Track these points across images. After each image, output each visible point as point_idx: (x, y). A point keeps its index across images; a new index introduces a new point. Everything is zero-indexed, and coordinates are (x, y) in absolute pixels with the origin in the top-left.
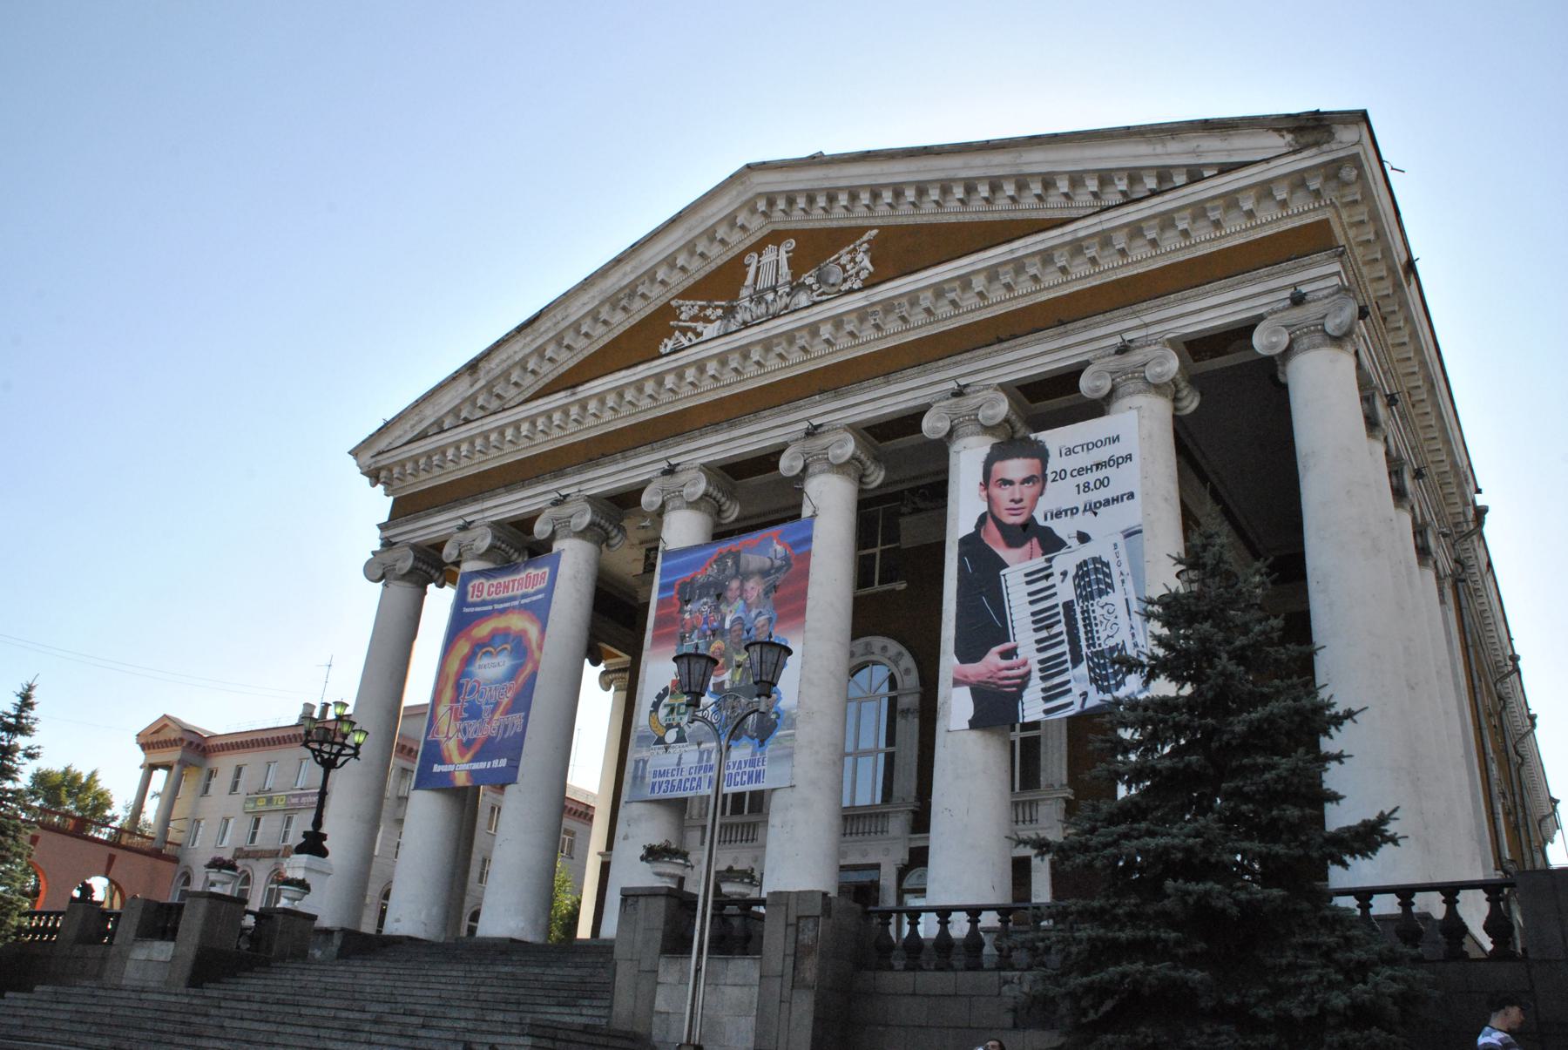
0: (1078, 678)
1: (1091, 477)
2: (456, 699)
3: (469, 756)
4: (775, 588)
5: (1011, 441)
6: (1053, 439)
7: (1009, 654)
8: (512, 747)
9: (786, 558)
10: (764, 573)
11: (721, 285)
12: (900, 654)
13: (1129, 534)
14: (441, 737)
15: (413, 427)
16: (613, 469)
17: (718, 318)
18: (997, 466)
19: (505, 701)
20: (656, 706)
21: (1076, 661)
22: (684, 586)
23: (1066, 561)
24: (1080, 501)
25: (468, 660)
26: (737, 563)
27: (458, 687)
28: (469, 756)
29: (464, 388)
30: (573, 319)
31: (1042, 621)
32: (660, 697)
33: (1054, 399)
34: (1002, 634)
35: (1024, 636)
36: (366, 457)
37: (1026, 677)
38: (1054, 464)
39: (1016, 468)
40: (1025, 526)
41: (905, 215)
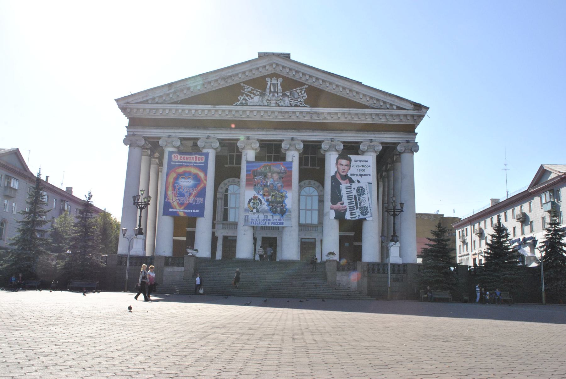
1: (361, 168)
3: (183, 207)
4: (283, 178)
6: (353, 157)
7: (342, 204)
8: (201, 207)
9: (285, 170)
10: (279, 173)
11: (259, 84)
13: (369, 183)
14: (171, 201)
16: (227, 132)
17: (258, 95)
18: (340, 160)
19: (194, 193)
20: (249, 202)
21: (357, 208)
24: (358, 173)
25: (176, 179)
26: (270, 168)
27: (174, 188)
28: (183, 207)
29: (165, 90)
30: (209, 80)
31: (349, 198)
33: (351, 149)
34: (340, 199)
35: (345, 201)
37: (346, 210)
38: (353, 163)
39: (344, 162)
40: (345, 176)
41: (316, 85)
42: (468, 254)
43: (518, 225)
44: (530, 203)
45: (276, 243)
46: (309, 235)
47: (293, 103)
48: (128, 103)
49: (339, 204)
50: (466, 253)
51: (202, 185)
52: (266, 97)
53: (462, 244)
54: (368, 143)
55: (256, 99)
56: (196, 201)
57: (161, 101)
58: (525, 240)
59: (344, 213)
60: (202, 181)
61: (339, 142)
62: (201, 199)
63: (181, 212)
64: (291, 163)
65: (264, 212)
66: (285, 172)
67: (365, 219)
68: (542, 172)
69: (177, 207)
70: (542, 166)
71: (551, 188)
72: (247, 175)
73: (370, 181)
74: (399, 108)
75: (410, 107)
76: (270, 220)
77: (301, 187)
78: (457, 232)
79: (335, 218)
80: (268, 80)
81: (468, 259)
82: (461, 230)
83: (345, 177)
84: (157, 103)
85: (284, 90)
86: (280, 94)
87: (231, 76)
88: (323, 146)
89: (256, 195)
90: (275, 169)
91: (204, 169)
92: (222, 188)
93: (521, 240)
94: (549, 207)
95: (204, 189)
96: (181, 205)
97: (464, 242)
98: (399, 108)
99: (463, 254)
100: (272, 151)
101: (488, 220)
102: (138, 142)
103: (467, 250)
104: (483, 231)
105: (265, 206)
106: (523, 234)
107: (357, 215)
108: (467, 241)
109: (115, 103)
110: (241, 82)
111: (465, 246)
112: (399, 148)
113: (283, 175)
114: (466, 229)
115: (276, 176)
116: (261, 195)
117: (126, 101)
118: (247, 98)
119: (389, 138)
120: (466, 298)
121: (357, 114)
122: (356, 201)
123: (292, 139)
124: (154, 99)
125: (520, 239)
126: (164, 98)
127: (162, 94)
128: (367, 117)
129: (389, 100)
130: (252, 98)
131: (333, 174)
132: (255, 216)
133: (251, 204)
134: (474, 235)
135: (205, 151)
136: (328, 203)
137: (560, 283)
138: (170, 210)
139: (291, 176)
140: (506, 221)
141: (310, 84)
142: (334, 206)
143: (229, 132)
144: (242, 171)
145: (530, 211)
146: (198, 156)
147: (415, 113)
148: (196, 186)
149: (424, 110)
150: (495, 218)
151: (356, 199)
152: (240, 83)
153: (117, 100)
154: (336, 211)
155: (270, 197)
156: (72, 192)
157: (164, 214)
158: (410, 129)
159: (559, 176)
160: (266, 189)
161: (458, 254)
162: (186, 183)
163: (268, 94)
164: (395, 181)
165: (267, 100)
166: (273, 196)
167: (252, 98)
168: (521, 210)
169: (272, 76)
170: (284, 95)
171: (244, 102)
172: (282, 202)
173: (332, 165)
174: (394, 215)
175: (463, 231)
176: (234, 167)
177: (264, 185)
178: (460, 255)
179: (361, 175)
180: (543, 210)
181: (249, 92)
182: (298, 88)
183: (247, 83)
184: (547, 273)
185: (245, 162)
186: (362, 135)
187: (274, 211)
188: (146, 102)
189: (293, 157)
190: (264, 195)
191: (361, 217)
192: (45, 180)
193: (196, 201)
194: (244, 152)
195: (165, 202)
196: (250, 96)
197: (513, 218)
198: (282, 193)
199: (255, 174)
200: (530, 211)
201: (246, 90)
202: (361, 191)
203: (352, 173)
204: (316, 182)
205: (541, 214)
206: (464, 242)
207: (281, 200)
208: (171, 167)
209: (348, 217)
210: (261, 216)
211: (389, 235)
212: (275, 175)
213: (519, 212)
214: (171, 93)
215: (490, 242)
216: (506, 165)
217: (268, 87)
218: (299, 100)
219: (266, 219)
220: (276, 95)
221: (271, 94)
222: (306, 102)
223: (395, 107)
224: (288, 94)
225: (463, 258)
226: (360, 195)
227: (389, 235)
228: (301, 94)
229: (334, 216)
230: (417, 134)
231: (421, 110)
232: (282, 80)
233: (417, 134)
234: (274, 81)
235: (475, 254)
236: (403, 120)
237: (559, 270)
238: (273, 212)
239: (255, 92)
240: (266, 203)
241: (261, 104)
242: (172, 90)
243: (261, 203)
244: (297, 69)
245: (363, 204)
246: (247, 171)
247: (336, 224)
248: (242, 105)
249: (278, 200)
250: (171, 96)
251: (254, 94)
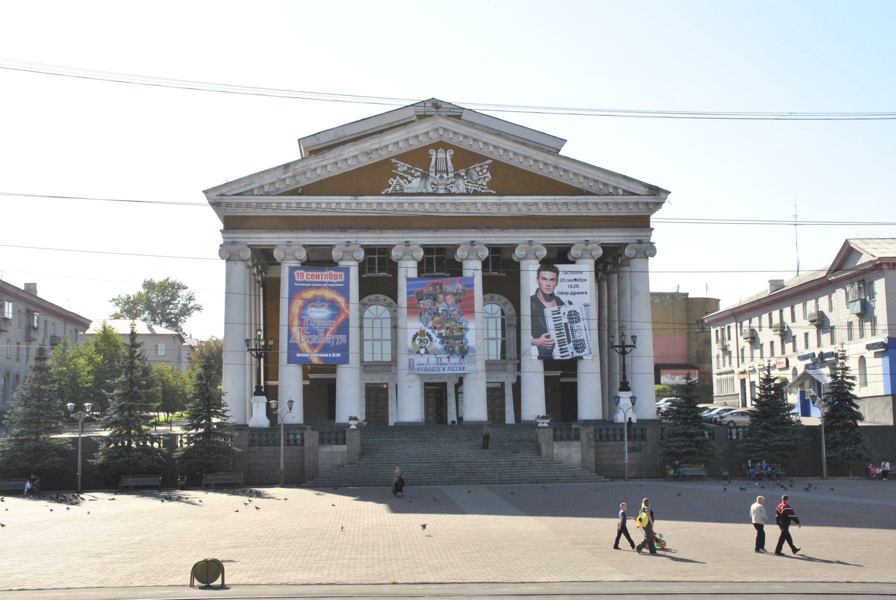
0: (570, 347)
1: (573, 283)
2: (301, 325)
3: (316, 350)
4: (460, 301)
5: (547, 264)
6: (561, 267)
7: (548, 337)
8: (344, 349)
9: (463, 290)
10: (455, 294)
11: (418, 158)
12: (506, 303)
13: (586, 306)
14: (297, 341)
15: (245, 186)
16: (375, 236)
17: (418, 176)
18: (542, 273)
19: (331, 329)
20: (414, 339)
21: (569, 342)
22: (418, 293)
23: (565, 309)
24: (570, 290)
25: (304, 308)
26: (441, 287)
27: (301, 321)
28: (316, 350)
29: (280, 175)
30: (345, 157)
31: (558, 328)
32: (415, 336)
33: (558, 256)
34: (545, 330)
35: (553, 333)
36: (214, 196)
37: (554, 345)
38: (561, 276)
39: (548, 274)
40: (551, 295)
41: (505, 159)
42: (733, 372)
43: (813, 331)
44: (830, 297)
45: (446, 391)
46: (376, 379)
47: (472, 188)
48: (223, 195)
49: (543, 338)
50: (728, 368)
51: (343, 316)
53: (721, 352)
54: (583, 246)
55: (416, 184)
56: (336, 341)
57: (272, 189)
58: (822, 355)
59: (552, 351)
60: (343, 311)
61: (540, 246)
62: (342, 338)
63: (315, 357)
64: (472, 279)
65: (436, 352)
66: (464, 292)
67: (581, 358)
68: (848, 252)
69: (308, 350)
70: (847, 242)
71: (861, 278)
72: (409, 299)
73: (587, 302)
74: (627, 193)
75: (644, 191)
76: (446, 364)
78: (713, 331)
79: (539, 358)
80: (432, 152)
81: (733, 379)
82: (719, 329)
83: (551, 297)
84: (267, 194)
85: (456, 169)
86: (451, 175)
87: (377, 150)
88: (516, 252)
89: (424, 328)
90: (448, 288)
91: (344, 291)
93: (817, 356)
94: (857, 307)
95: (346, 321)
96: (313, 346)
97: (725, 350)
98: (627, 193)
99: (723, 370)
100: (440, 263)
101: (765, 317)
102: (241, 254)
103: (730, 364)
104: (757, 334)
105: (437, 344)
106: (819, 345)
107: (569, 353)
108: (730, 349)
109: (204, 196)
110: (392, 157)
111: (727, 359)
112: (627, 252)
113: (462, 298)
114: (729, 328)
115: (450, 299)
116: (430, 328)
117: (219, 192)
118: (402, 182)
119: (612, 237)
120: (726, 474)
121: (566, 204)
122: (567, 331)
123: (472, 243)
125: (814, 354)
126: (277, 186)
127: (275, 179)
128: (580, 207)
129: (612, 181)
130: (410, 182)
131: (533, 293)
132: (423, 360)
133: (417, 342)
134: (741, 339)
135: (343, 264)
136: (527, 337)
137: (847, 448)
138: (298, 355)
139: (472, 298)
140: (793, 320)
142: (537, 340)
143: (379, 235)
144: (399, 293)
145: (831, 310)
146: (334, 273)
147: (651, 199)
148: (333, 317)
149: (662, 195)
150: (776, 314)
151: (567, 330)
152: (389, 159)
153: (205, 192)
154: (540, 348)
155: (443, 331)
156: (36, 291)
157: (289, 362)
158: (643, 223)
159: (871, 262)
160: (437, 318)
161: (715, 371)
162: (319, 314)
163: (433, 174)
164: (621, 294)
165: (432, 184)
166: (448, 328)
167: (410, 182)
168: (817, 306)
170: (457, 176)
171: (398, 188)
172: (462, 337)
173: (531, 280)
174: (623, 353)
175: (723, 330)
176: (375, 278)
177: (435, 314)
178: (718, 371)
179: (574, 294)
180: (848, 311)
181: (404, 172)
182: (478, 165)
183: (400, 157)
184: (831, 436)
185: (405, 280)
186: (573, 235)
187: (450, 352)
188: (251, 192)
189: (473, 269)
190: (435, 328)
191: (576, 354)
192: (149, 332)
193: (336, 341)
194: (524, 265)
195: (289, 344)
196: (407, 178)
197: (805, 318)
198: (460, 324)
199: (420, 296)
200: (831, 310)
201: (399, 169)
202: (574, 317)
203: (561, 290)
204: (501, 297)
205: (847, 316)
206: (725, 350)
207: (459, 334)
208: (295, 291)
209: (557, 355)
210: (432, 359)
211: (617, 382)
212: (448, 297)
213: (813, 311)
214: (288, 178)
215: (757, 397)
217: (433, 163)
218: (479, 183)
219: (439, 363)
220: (445, 176)
221: (438, 175)
222: (490, 185)
223: (621, 192)
224: (463, 174)
225: (724, 376)
226: (573, 322)
227: (617, 382)
228: (482, 175)
229: (537, 353)
230: (653, 229)
231: (659, 194)
232: (452, 152)
233: (653, 229)
234: (441, 155)
235: (743, 373)
236: (633, 210)
237: (847, 431)
238: (448, 352)
239: (413, 172)
240: (438, 340)
241: (424, 191)
242: (290, 174)
243: (431, 339)
244: (475, 137)
245: (578, 336)
246: (408, 293)
247: (540, 365)
248: (395, 194)
249: (456, 334)
250: (288, 182)
251: (412, 175)
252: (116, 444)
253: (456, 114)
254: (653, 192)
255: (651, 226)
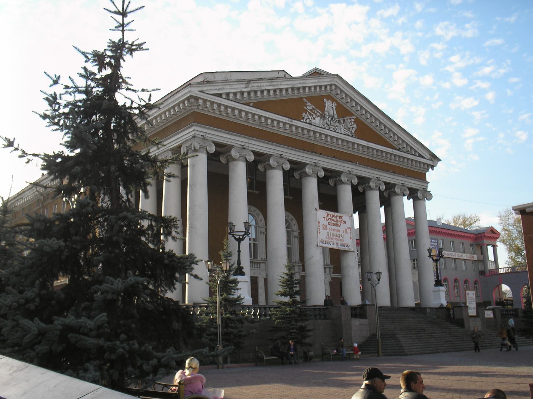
11: (318, 102)
15: (219, 89)
52: (326, 121)
77: (343, 213)
92: (254, 211)
98: (420, 156)
118: (310, 117)
124: (228, 94)
141: (358, 116)
169: (329, 97)
181: (310, 110)
216: (10, 144)
252: (121, 296)
253: (341, 78)
254: (433, 159)
255: (427, 180)
